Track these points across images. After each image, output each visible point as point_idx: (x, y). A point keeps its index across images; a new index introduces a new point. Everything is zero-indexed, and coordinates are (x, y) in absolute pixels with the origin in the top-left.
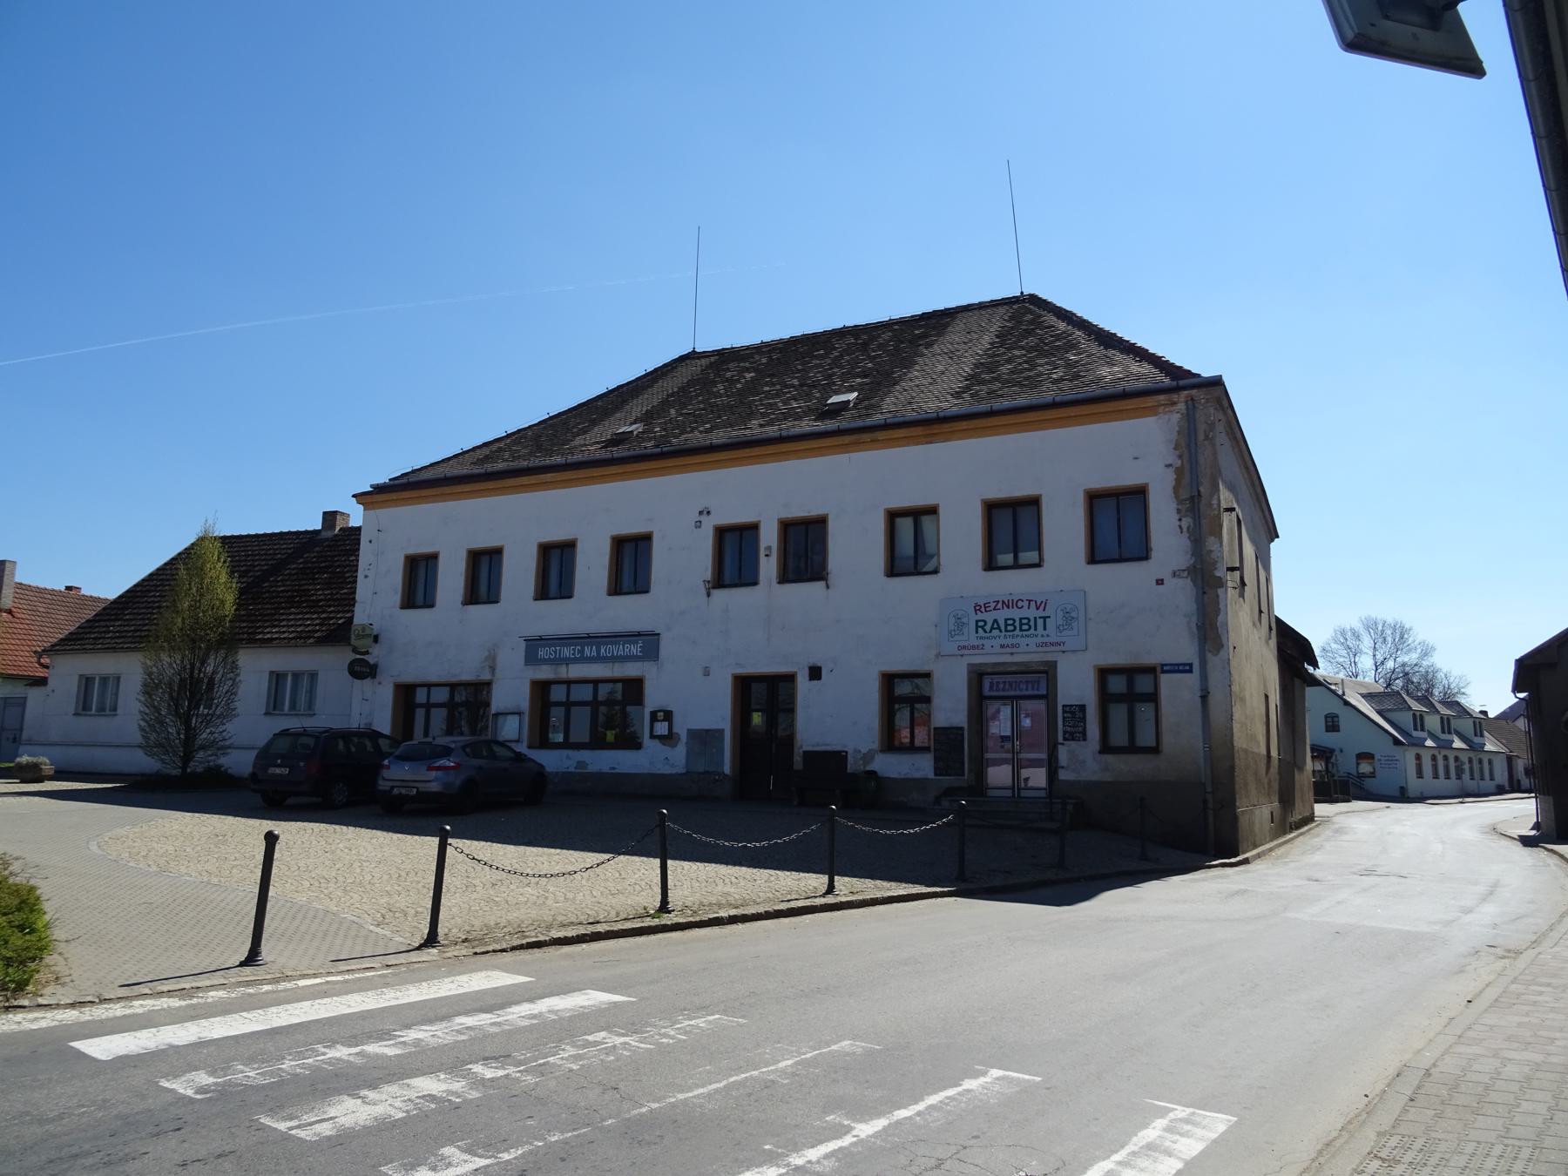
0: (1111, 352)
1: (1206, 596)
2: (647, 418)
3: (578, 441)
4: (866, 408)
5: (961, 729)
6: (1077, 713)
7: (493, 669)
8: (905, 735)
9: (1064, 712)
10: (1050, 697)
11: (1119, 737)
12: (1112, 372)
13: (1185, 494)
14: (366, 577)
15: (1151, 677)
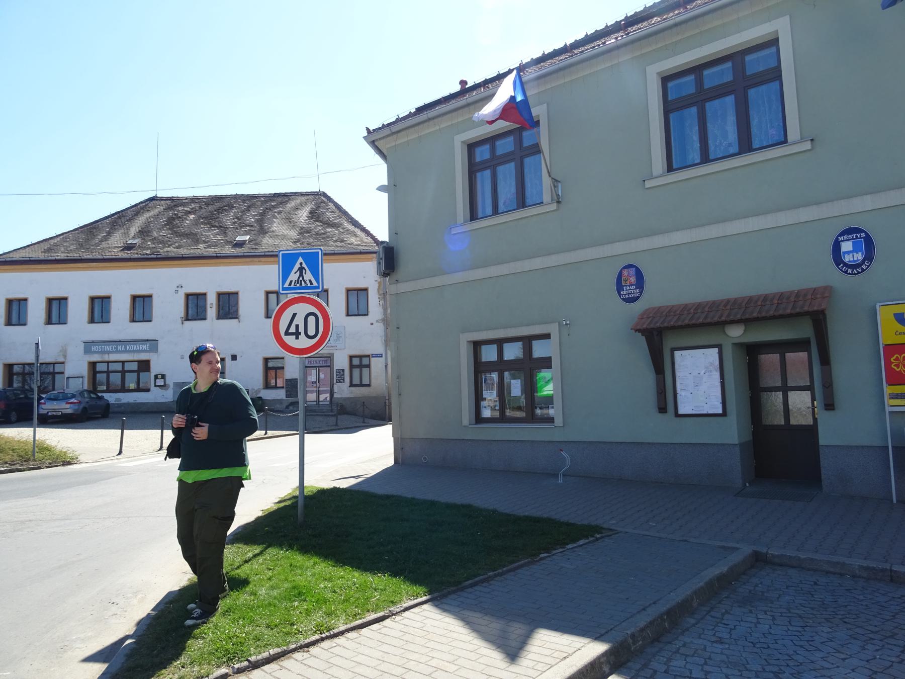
0: (357, 230)
2: (141, 234)
3: (104, 245)
5: (809, 338)
7: (65, 356)
8: (273, 382)
9: (336, 372)
10: (331, 366)
11: (356, 381)
12: (357, 240)
13: (381, 292)
15: (368, 358)
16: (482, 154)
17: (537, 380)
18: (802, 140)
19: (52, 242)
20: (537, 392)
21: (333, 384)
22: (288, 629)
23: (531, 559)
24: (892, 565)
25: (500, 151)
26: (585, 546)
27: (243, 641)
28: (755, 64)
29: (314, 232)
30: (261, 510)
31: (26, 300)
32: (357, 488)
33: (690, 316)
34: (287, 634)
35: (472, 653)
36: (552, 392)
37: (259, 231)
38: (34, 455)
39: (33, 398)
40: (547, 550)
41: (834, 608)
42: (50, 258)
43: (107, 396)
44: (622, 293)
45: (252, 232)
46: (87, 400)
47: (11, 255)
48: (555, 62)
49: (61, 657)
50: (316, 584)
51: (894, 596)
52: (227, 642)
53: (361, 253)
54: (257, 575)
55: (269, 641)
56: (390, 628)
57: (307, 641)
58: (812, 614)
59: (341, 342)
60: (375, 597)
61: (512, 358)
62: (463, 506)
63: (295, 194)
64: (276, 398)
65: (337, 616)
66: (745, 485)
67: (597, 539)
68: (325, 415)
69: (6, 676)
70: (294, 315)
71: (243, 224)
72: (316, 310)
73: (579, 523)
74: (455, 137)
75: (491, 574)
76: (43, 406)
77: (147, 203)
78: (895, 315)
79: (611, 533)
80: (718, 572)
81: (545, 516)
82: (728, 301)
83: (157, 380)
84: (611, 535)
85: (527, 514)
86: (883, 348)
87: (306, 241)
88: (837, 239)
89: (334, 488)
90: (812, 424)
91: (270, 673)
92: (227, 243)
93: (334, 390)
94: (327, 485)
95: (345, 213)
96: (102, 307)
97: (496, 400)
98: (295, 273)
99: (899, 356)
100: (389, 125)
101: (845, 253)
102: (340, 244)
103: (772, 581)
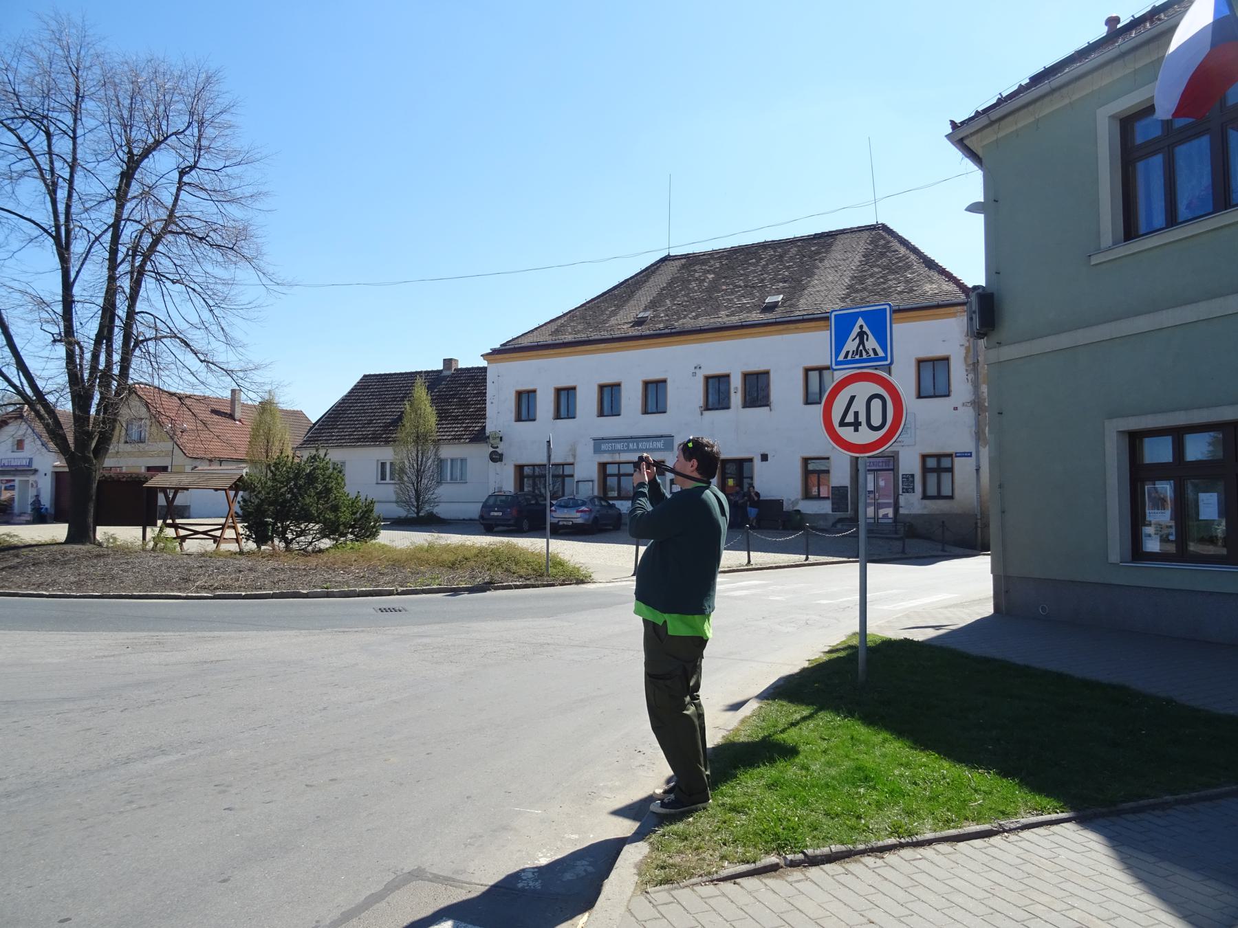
1: (980, 417)
2: (653, 305)
3: (613, 321)
4: (790, 306)
5: (847, 487)
6: (910, 478)
7: (574, 456)
8: (814, 491)
9: (903, 478)
10: (894, 470)
11: (932, 491)
12: (932, 288)
14: (492, 403)
15: (950, 459)
19: (560, 322)
22: (853, 822)
27: (796, 827)
29: (870, 281)
30: (807, 659)
31: (534, 391)
34: (852, 828)
35: (1141, 915)
37: (796, 287)
38: (547, 570)
39: (545, 505)
42: (557, 341)
43: (618, 504)
45: (787, 290)
46: (598, 508)
47: (520, 341)
49: (590, 804)
50: (889, 769)
52: (775, 823)
53: (938, 306)
54: (807, 744)
55: (829, 833)
56: (1000, 849)
57: (880, 843)
59: (909, 435)
60: (976, 801)
64: (818, 513)
65: (920, 817)
68: (887, 538)
69: (537, 814)
70: (853, 398)
71: (774, 280)
72: (882, 389)
74: (1098, 111)
75: (1168, 798)
76: (554, 514)
77: (658, 265)
83: (673, 486)
87: (858, 296)
89: (906, 639)
91: (833, 876)
92: (755, 307)
94: (896, 633)
95: (915, 250)
96: (612, 397)
97: (1170, 524)
98: (853, 340)
100: (986, 111)
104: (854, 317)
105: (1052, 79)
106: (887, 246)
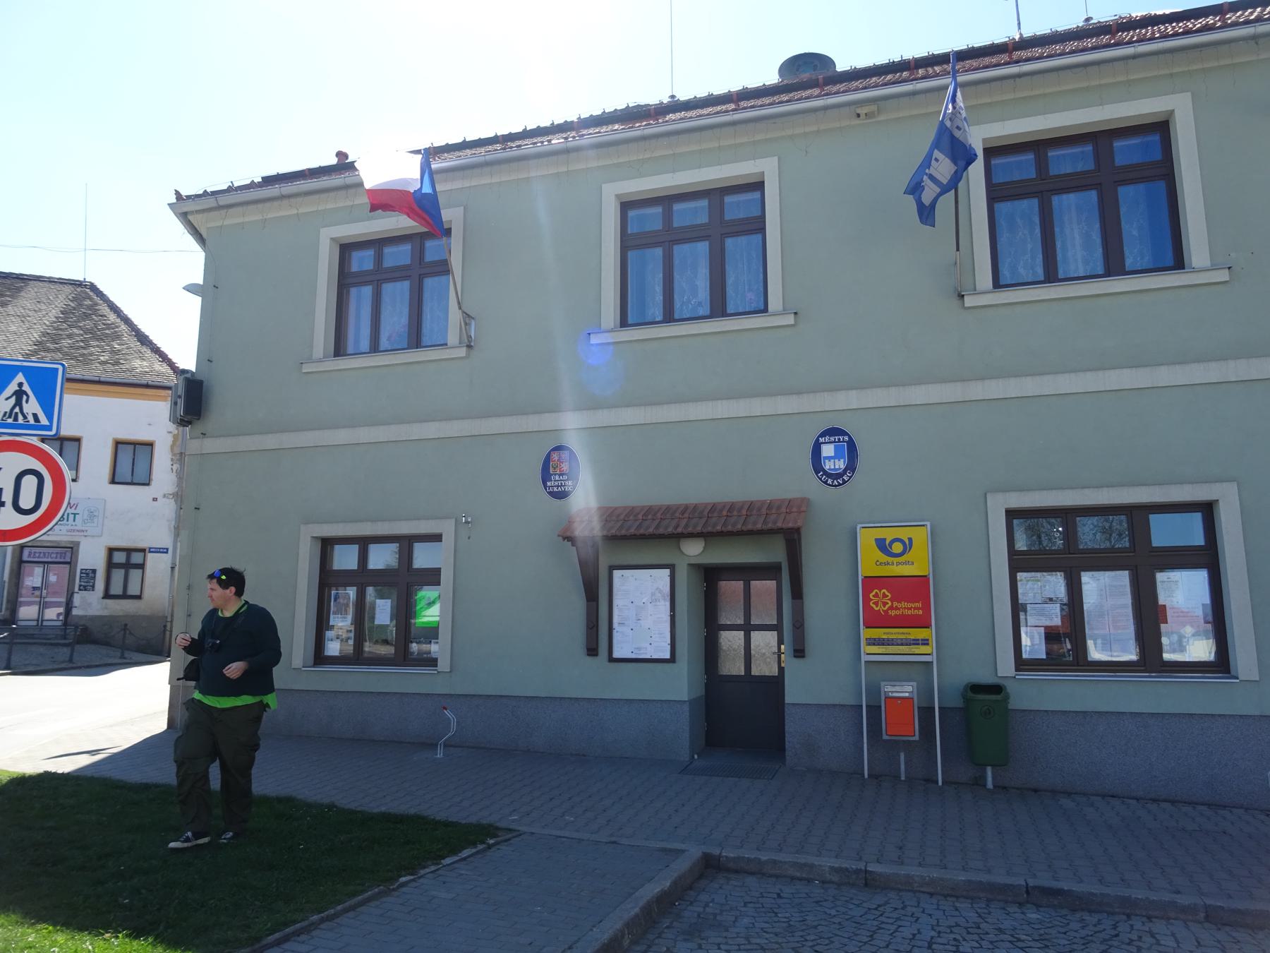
0: (144, 349)
1: (182, 511)
5: (780, 563)
6: (90, 574)
9: (81, 573)
10: (71, 563)
11: (116, 589)
12: (142, 365)
13: (177, 450)
15: (142, 554)
16: (362, 261)
17: (416, 600)
18: (784, 312)
20: (415, 617)
21: (73, 593)
23: (384, 886)
24: (867, 863)
25: (388, 263)
26: (472, 859)
28: (736, 207)
29: (66, 342)
32: (89, 774)
33: (638, 523)
36: (437, 619)
40: (411, 869)
41: (803, 930)
44: (549, 484)
48: (481, 153)
51: (870, 907)
53: (147, 386)
58: (777, 943)
59: (95, 525)
61: (380, 566)
62: (279, 800)
63: (38, 279)
66: (693, 757)
67: (490, 847)
68: (52, 644)
73: (464, 822)
75: (315, 918)
78: (877, 540)
79: (510, 836)
80: (658, 890)
81: (412, 811)
82: (686, 507)
84: (509, 840)
85: (383, 809)
86: (862, 580)
88: (817, 440)
90: (777, 674)
93: (72, 602)
95: (127, 321)
98: (7, 399)
99: (878, 591)
100: (214, 193)
101: (825, 458)
102: (112, 368)
103: (726, 896)
104: (13, 371)
105: (282, 185)
106: (92, 307)
